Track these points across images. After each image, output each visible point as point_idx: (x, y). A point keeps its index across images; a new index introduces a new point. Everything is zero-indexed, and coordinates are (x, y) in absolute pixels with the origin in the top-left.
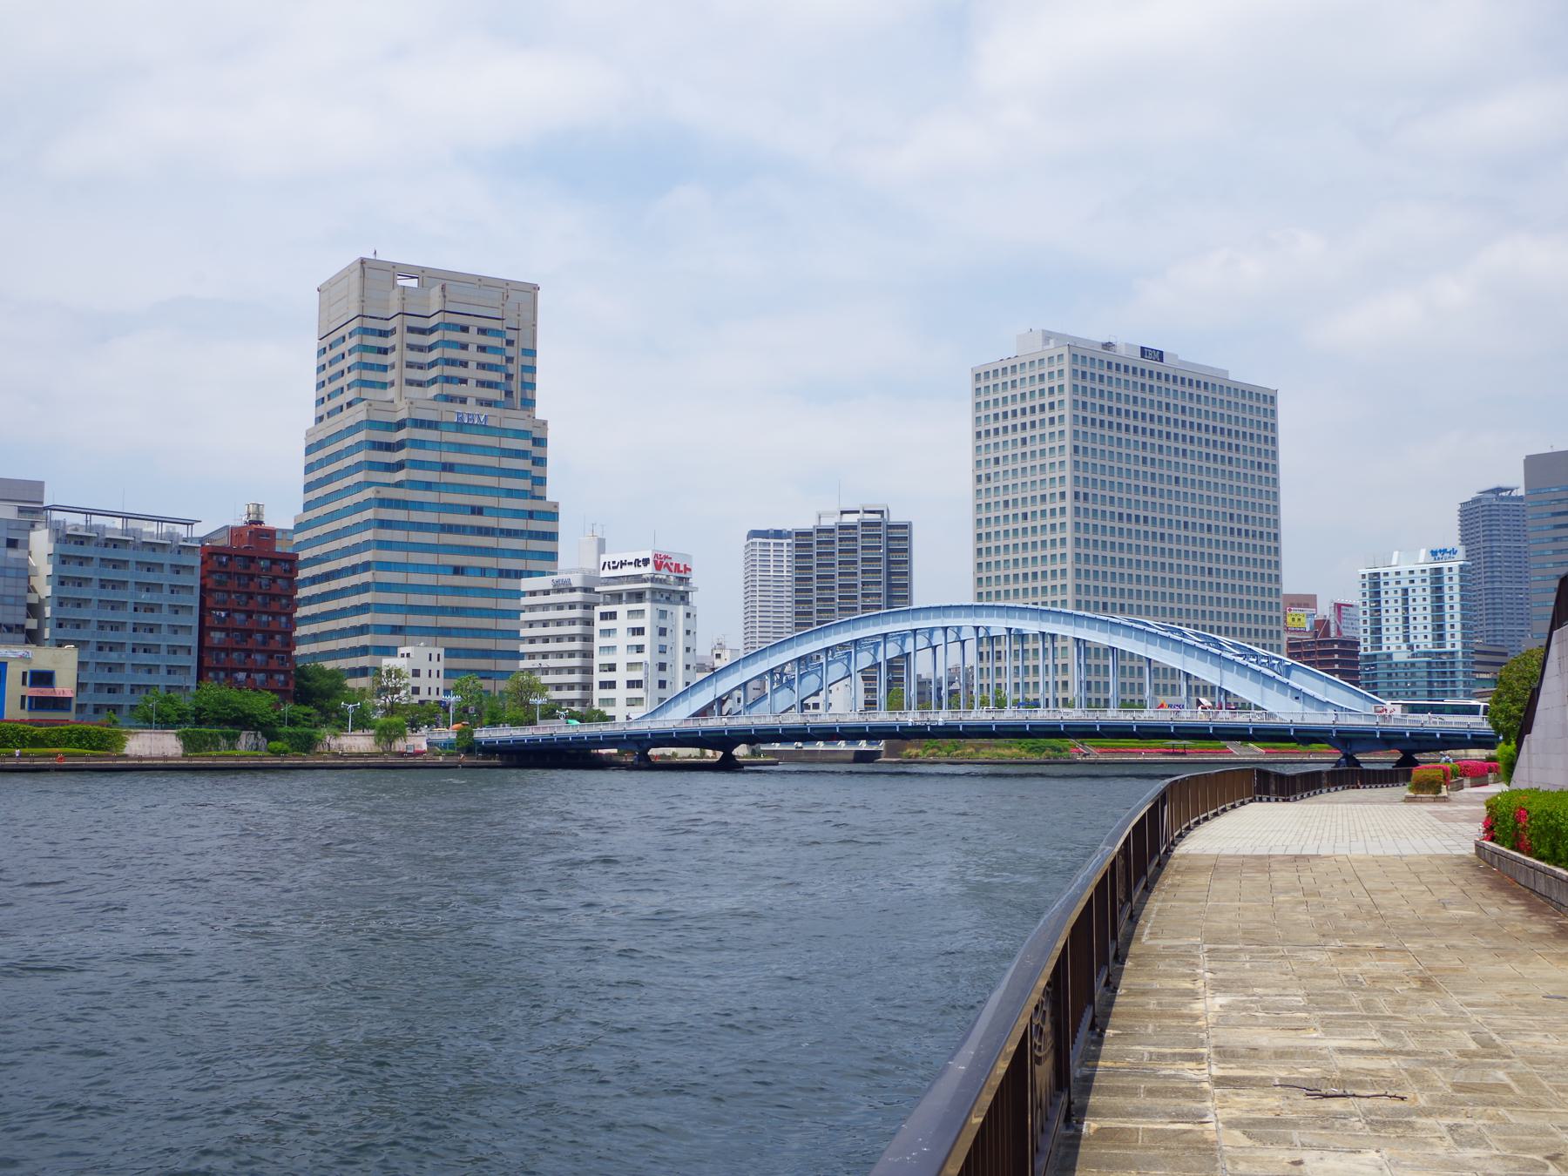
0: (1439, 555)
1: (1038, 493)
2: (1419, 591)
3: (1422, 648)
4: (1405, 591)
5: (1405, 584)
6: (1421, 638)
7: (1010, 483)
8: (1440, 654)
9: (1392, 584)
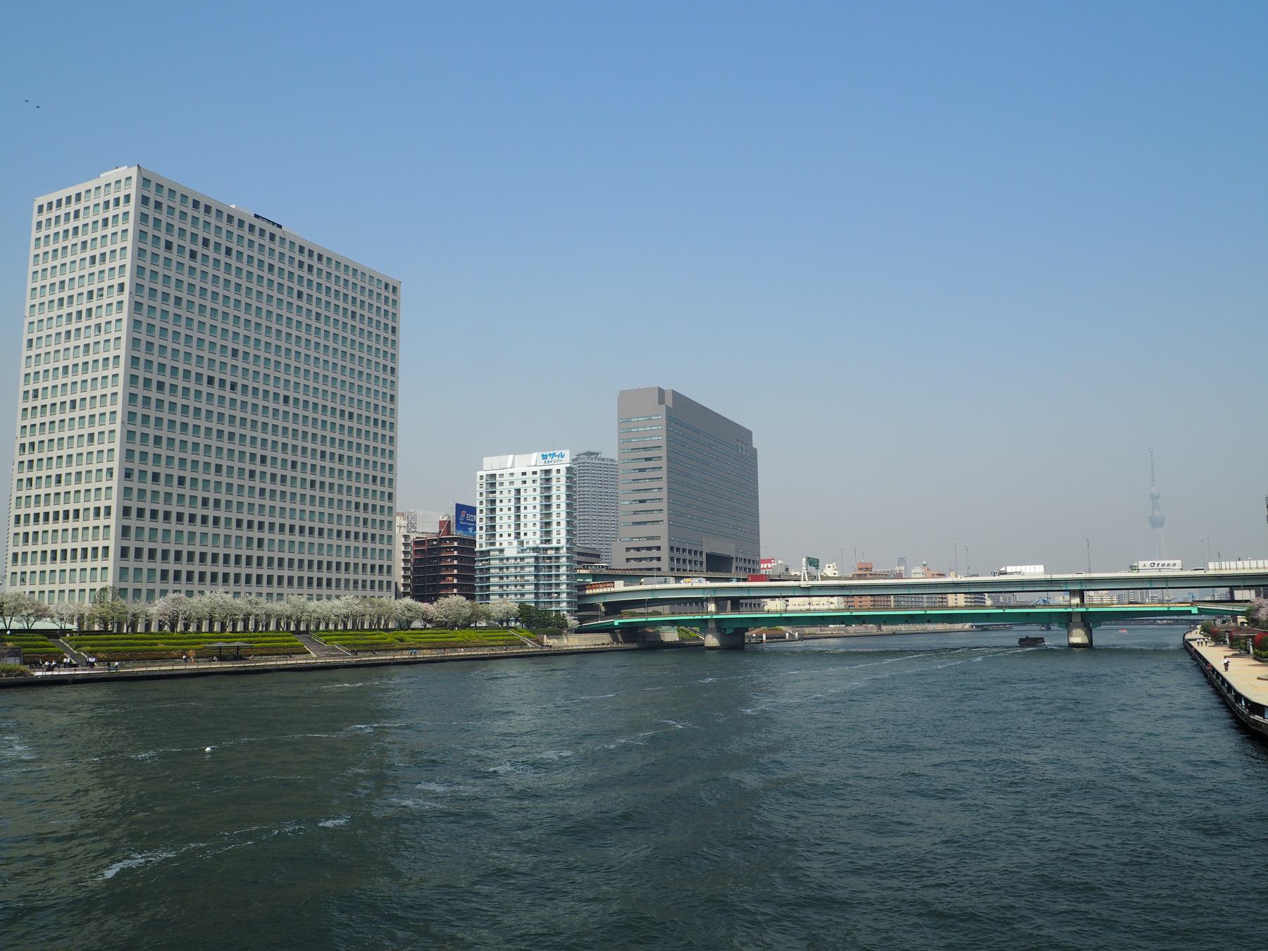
0: (549, 458)
2: (530, 491)
3: (531, 545)
4: (518, 491)
5: (518, 485)
6: (530, 535)
8: (546, 549)
9: (506, 485)
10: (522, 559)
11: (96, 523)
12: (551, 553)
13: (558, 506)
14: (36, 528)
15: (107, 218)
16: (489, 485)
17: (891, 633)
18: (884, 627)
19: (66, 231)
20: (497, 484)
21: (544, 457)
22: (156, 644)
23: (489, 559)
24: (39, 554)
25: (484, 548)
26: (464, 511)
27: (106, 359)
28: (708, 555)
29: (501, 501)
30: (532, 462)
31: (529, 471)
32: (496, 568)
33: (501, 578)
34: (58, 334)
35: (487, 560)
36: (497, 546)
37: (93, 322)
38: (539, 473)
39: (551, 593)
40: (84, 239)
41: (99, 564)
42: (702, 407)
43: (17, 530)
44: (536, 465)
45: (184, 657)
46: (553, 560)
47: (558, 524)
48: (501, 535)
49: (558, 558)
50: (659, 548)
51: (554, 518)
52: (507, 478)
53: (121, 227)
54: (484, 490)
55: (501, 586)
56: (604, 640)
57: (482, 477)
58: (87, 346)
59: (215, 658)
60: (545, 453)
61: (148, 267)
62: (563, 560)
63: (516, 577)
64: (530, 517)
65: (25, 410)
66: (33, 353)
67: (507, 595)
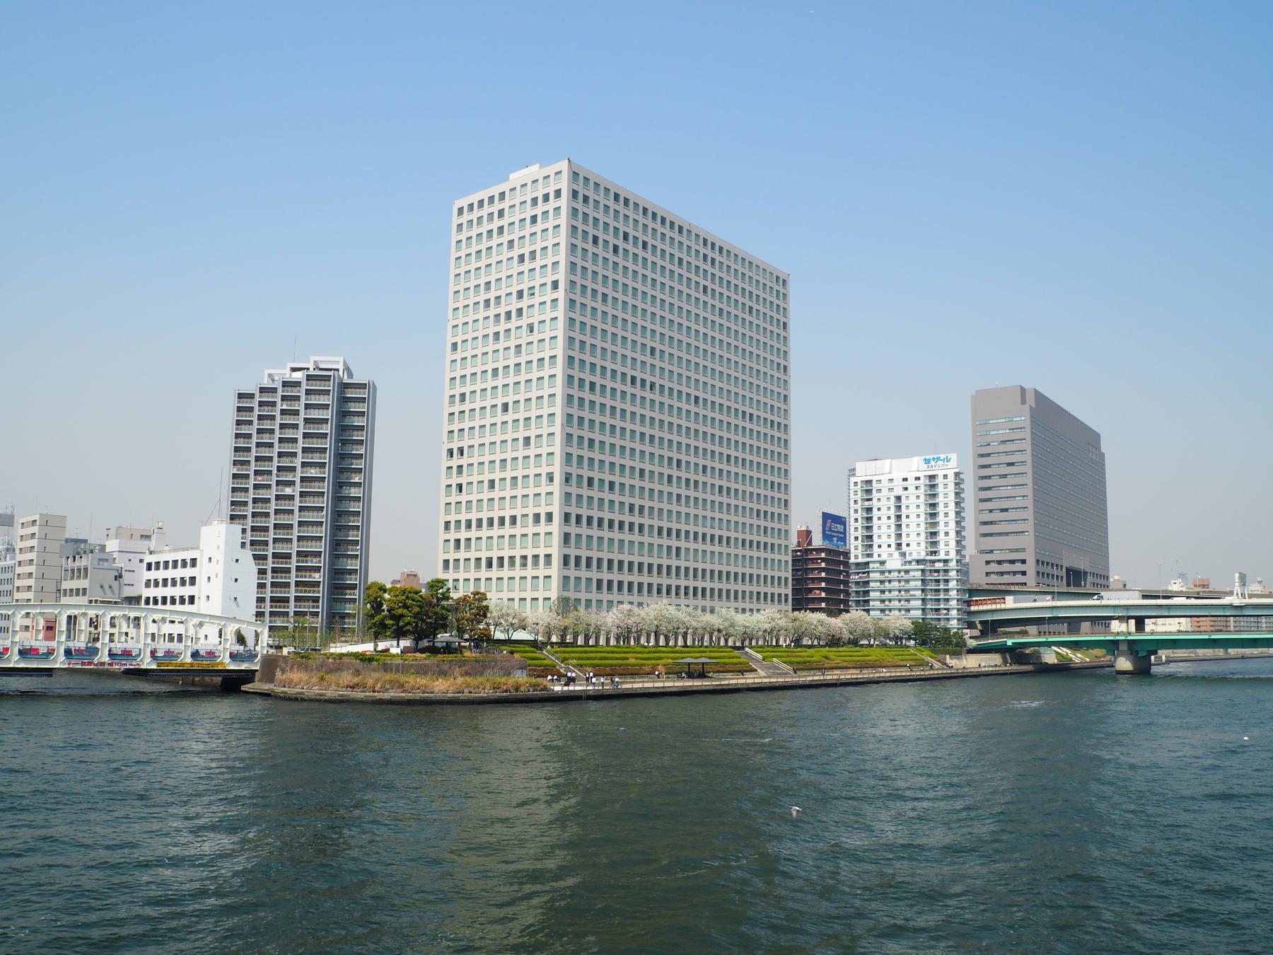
0: (933, 463)
1: (497, 457)
2: (913, 499)
3: (915, 556)
4: (898, 498)
5: (899, 491)
6: (913, 546)
7: (466, 425)
8: (933, 562)
9: (885, 492)
10: (907, 572)
11: (536, 530)
12: (939, 566)
13: (946, 515)
14: (468, 535)
15: (536, 216)
16: (864, 492)
17: (1240, 656)
18: (1230, 650)
19: (490, 232)
20: (874, 491)
21: (927, 461)
22: (627, 659)
23: (868, 572)
24: (473, 561)
25: (860, 560)
26: (833, 523)
27: (541, 360)
28: (1068, 570)
29: (879, 509)
30: (914, 466)
31: (911, 477)
32: (876, 581)
33: (883, 592)
34: (486, 336)
35: (864, 573)
36: (875, 558)
37: (524, 322)
38: (859, 484)
39: (939, 609)
40: (510, 238)
41: (541, 572)
42: (1060, 407)
43: (447, 537)
44: (918, 471)
45: (657, 673)
46: (942, 573)
47: (947, 534)
48: (880, 546)
49: (946, 571)
50: (1023, 562)
51: (941, 528)
52: (885, 484)
53: (551, 224)
54: (859, 497)
55: (883, 601)
56: (990, 662)
57: (856, 484)
58: (518, 347)
59: (683, 675)
60: (927, 457)
61: (580, 263)
62: (953, 574)
63: (900, 591)
64: (913, 527)
65: (452, 414)
66: (458, 356)
67: (890, 610)
